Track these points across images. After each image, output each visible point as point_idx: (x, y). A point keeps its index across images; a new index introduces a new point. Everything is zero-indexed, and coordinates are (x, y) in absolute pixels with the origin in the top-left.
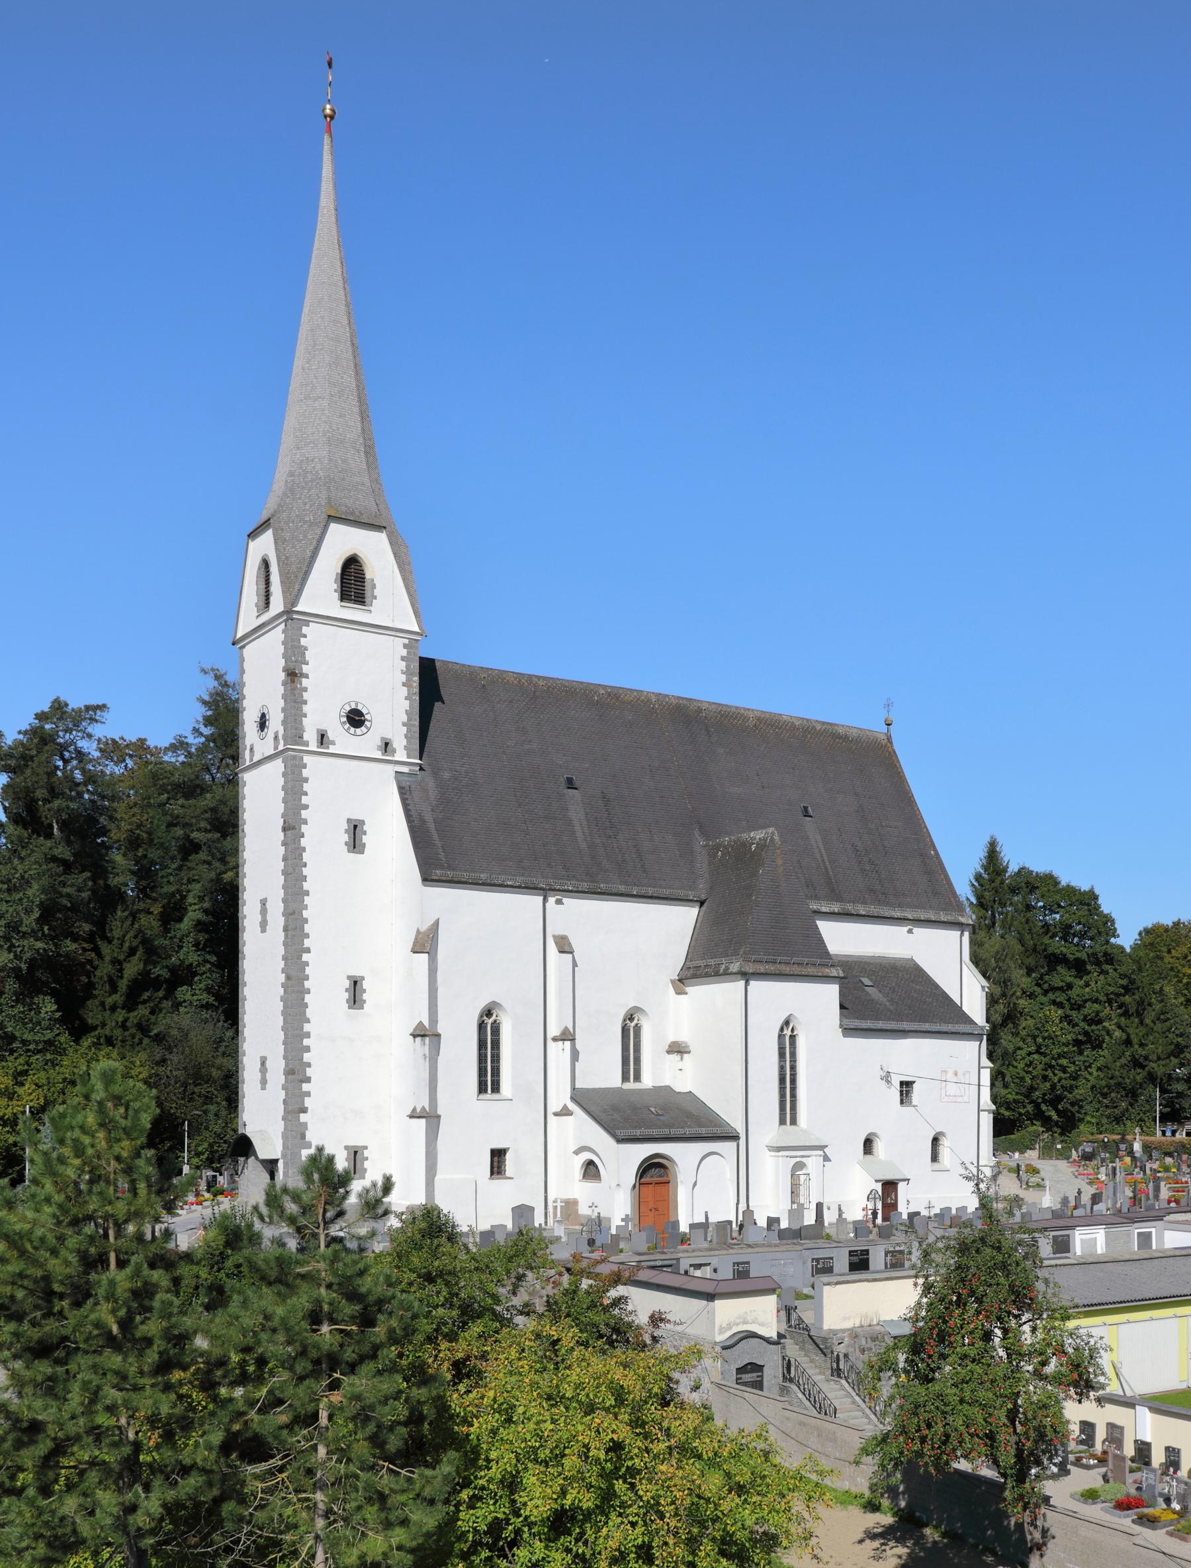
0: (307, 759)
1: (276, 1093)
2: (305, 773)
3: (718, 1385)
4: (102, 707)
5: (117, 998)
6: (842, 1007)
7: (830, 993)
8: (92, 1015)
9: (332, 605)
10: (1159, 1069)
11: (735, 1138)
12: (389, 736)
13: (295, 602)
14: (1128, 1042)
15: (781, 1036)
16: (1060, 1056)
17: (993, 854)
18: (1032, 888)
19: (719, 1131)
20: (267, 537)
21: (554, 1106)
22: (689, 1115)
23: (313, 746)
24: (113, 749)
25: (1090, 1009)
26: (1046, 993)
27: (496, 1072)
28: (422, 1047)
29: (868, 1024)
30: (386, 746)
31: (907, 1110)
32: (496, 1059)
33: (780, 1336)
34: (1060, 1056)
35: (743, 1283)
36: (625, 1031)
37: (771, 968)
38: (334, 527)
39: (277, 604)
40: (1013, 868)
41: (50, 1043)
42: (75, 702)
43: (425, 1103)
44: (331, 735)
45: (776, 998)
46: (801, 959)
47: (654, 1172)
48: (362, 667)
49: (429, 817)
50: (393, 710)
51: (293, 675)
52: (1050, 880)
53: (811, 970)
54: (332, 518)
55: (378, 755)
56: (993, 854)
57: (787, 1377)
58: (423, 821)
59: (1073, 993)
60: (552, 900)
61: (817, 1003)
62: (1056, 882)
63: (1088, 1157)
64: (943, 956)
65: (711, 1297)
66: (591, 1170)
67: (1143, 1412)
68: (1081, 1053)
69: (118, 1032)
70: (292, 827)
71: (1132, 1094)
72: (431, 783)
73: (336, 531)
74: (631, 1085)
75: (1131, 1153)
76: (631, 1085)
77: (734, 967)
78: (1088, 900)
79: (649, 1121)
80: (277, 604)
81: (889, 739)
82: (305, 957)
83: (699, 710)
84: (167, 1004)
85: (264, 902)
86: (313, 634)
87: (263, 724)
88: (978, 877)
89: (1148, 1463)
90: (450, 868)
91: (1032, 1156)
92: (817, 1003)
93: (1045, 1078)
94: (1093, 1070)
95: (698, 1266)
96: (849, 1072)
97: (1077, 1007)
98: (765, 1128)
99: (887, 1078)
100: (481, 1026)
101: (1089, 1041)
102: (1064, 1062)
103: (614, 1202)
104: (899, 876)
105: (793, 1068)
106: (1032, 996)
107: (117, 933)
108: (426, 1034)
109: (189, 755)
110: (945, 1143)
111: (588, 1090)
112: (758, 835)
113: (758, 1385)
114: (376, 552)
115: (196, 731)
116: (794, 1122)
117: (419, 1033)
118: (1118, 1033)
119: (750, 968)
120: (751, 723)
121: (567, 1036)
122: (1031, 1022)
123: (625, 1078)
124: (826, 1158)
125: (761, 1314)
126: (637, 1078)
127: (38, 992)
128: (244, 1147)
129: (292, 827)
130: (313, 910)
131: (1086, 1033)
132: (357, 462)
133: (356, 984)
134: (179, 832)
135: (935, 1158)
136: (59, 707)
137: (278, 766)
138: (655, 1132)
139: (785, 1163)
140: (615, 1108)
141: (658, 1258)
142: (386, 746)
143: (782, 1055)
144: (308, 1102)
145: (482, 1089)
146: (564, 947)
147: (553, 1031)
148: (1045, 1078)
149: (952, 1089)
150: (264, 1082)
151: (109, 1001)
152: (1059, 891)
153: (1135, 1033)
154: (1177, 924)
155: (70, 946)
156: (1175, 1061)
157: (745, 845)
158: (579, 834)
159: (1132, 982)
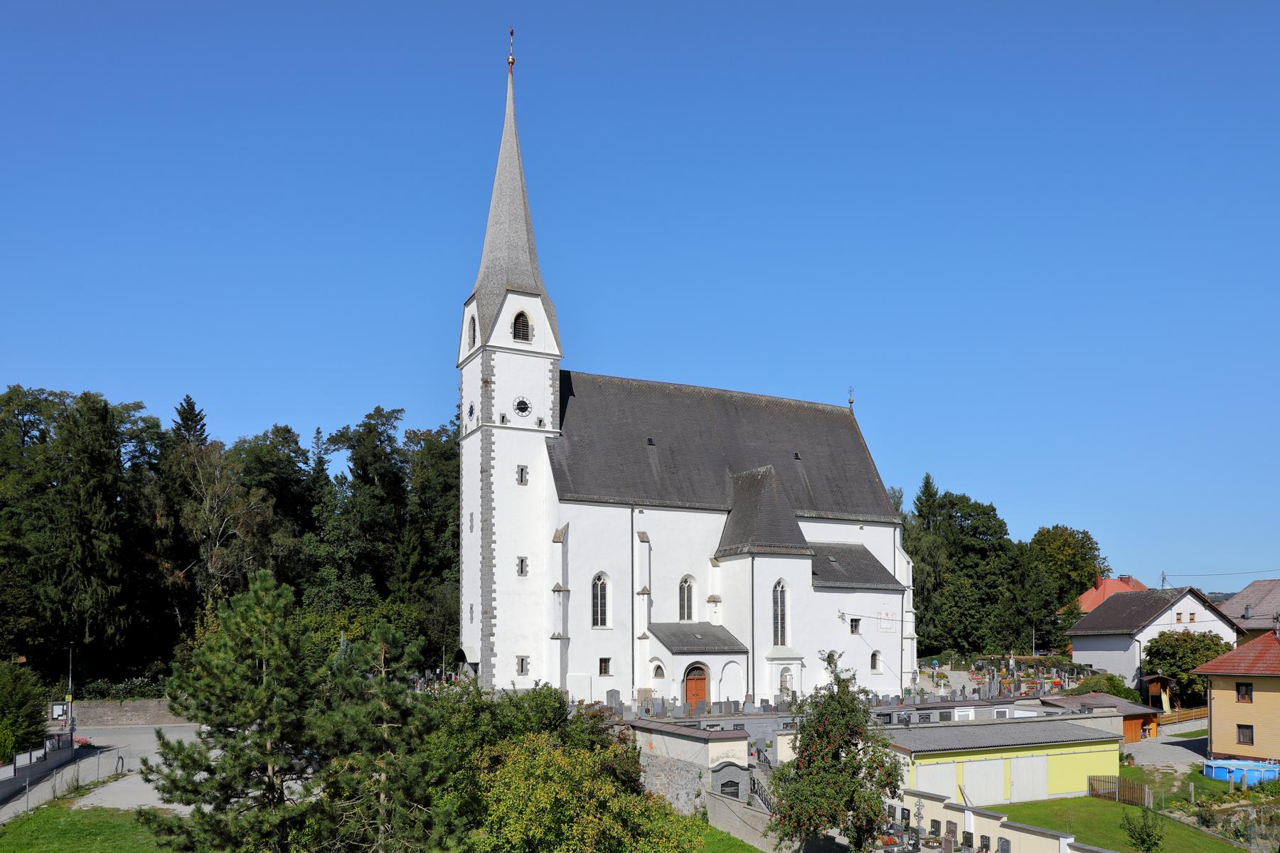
0: (494, 431)
1: (478, 624)
2: (493, 439)
3: (710, 794)
4: (401, 411)
5: (406, 575)
6: (814, 573)
7: (806, 565)
8: (392, 585)
9: (510, 342)
10: (1034, 616)
11: (746, 652)
12: (542, 416)
13: (487, 341)
14: (1014, 599)
15: (775, 591)
16: (970, 608)
17: (928, 484)
18: (953, 505)
19: (736, 649)
20: (474, 304)
21: (637, 634)
22: (719, 639)
23: (498, 423)
24: (412, 437)
25: (990, 578)
26: (961, 570)
27: (604, 613)
28: (558, 598)
29: (831, 584)
30: (540, 422)
31: (855, 636)
32: (604, 605)
33: (750, 766)
34: (970, 608)
35: (738, 733)
36: (682, 589)
37: (768, 550)
38: (510, 296)
39: (478, 343)
40: (941, 493)
41: (369, 600)
42: (387, 408)
43: (560, 630)
44: (508, 417)
45: (771, 568)
46: (792, 546)
47: (695, 673)
48: (527, 377)
49: (564, 463)
50: (544, 401)
51: (487, 383)
52: (964, 499)
53: (794, 551)
54: (508, 291)
55: (536, 428)
56: (928, 484)
57: (753, 791)
58: (561, 465)
59: (979, 569)
60: (637, 511)
61: (798, 572)
62: (968, 499)
63: (979, 669)
64: (883, 543)
65: (706, 741)
66: (659, 671)
67: (969, 814)
68: (984, 606)
69: (406, 595)
70: (486, 471)
71: (1017, 632)
72: (566, 443)
73: (511, 298)
74: (685, 621)
75: (1007, 666)
76: (685, 621)
77: (746, 550)
78: (989, 512)
79: (694, 642)
80: (478, 343)
81: (851, 411)
82: (493, 546)
83: (732, 397)
84: (435, 580)
85: (472, 515)
86: (498, 359)
87: (471, 413)
88: (919, 499)
89: (971, 846)
90: (576, 492)
91: (946, 669)
92: (798, 572)
93: (961, 622)
94: (992, 617)
95: (713, 726)
96: (819, 617)
97: (981, 578)
98: (764, 646)
99: (842, 617)
100: (594, 586)
101: (989, 598)
102: (972, 612)
103: (671, 689)
104: (859, 494)
105: (783, 611)
106: (953, 571)
107: (406, 538)
108: (561, 590)
109: (448, 436)
110: (880, 658)
111: (658, 624)
112: (762, 470)
113: (736, 795)
114: (534, 309)
115: (452, 422)
116: (783, 643)
117: (557, 590)
118: (1007, 594)
119: (755, 550)
120: (763, 404)
121: (646, 592)
122: (952, 587)
123: (682, 617)
124: (803, 666)
125: (738, 752)
126: (690, 617)
127: (362, 572)
128: (461, 656)
129: (486, 471)
130: (497, 519)
131: (987, 594)
132: (525, 258)
133: (522, 561)
134: (441, 479)
135: (874, 666)
136: (378, 411)
137: (478, 435)
138: (696, 649)
139: (777, 668)
140: (674, 635)
141: (688, 721)
142: (540, 422)
143: (775, 603)
144: (495, 630)
145: (595, 623)
146: (644, 539)
147: (637, 589)
148: (961, 622)
149: (885, 624)
150: (472, 619)
151: (402, 576)
152: (969, 506)
153: (1019, 593)
154: (1056, 528)
155: (381, 546)
156: (1044, 611)
157: (754, 476)
158: (655, 472)
159: (1017, 562)
